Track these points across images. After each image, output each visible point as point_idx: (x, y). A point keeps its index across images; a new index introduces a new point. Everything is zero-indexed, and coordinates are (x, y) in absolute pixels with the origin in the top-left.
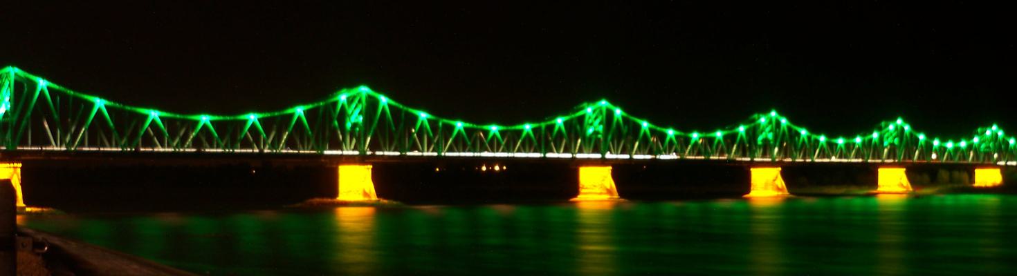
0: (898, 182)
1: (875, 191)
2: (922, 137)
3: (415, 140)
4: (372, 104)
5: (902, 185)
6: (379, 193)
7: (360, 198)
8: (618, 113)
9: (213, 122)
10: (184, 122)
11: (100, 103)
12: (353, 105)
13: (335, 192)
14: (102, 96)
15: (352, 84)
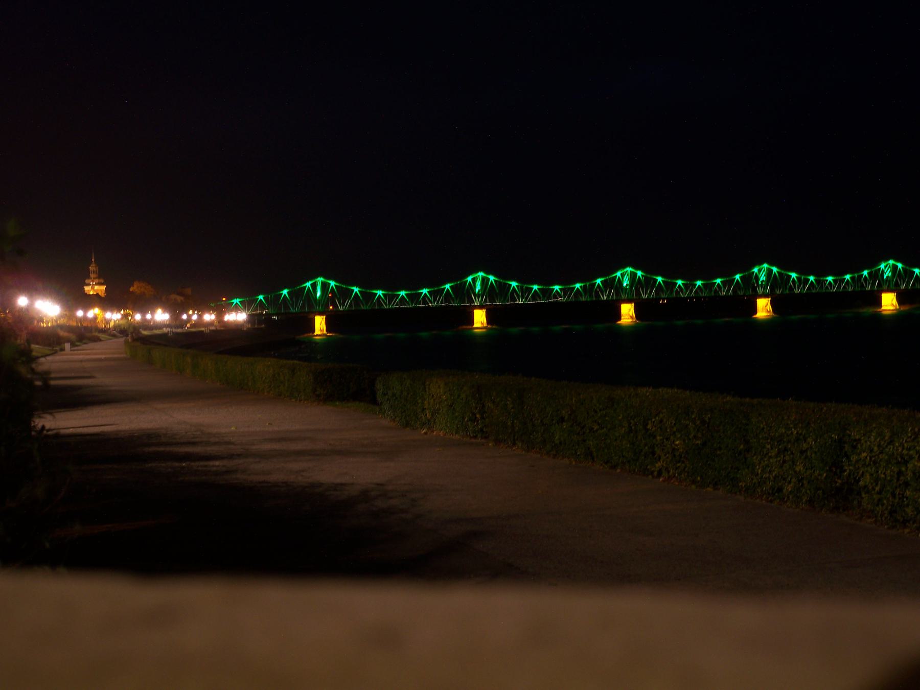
0: (890, 302)
1: (880, 310)
3: (862, 283)
6: (488, 323)
8: (900, 266)
9: (406, 294)
10: (569, 289)
11: (356, 290)
12: (887, 268)
13: (473, 324)
14: (357, 286)
15: (761, 263)
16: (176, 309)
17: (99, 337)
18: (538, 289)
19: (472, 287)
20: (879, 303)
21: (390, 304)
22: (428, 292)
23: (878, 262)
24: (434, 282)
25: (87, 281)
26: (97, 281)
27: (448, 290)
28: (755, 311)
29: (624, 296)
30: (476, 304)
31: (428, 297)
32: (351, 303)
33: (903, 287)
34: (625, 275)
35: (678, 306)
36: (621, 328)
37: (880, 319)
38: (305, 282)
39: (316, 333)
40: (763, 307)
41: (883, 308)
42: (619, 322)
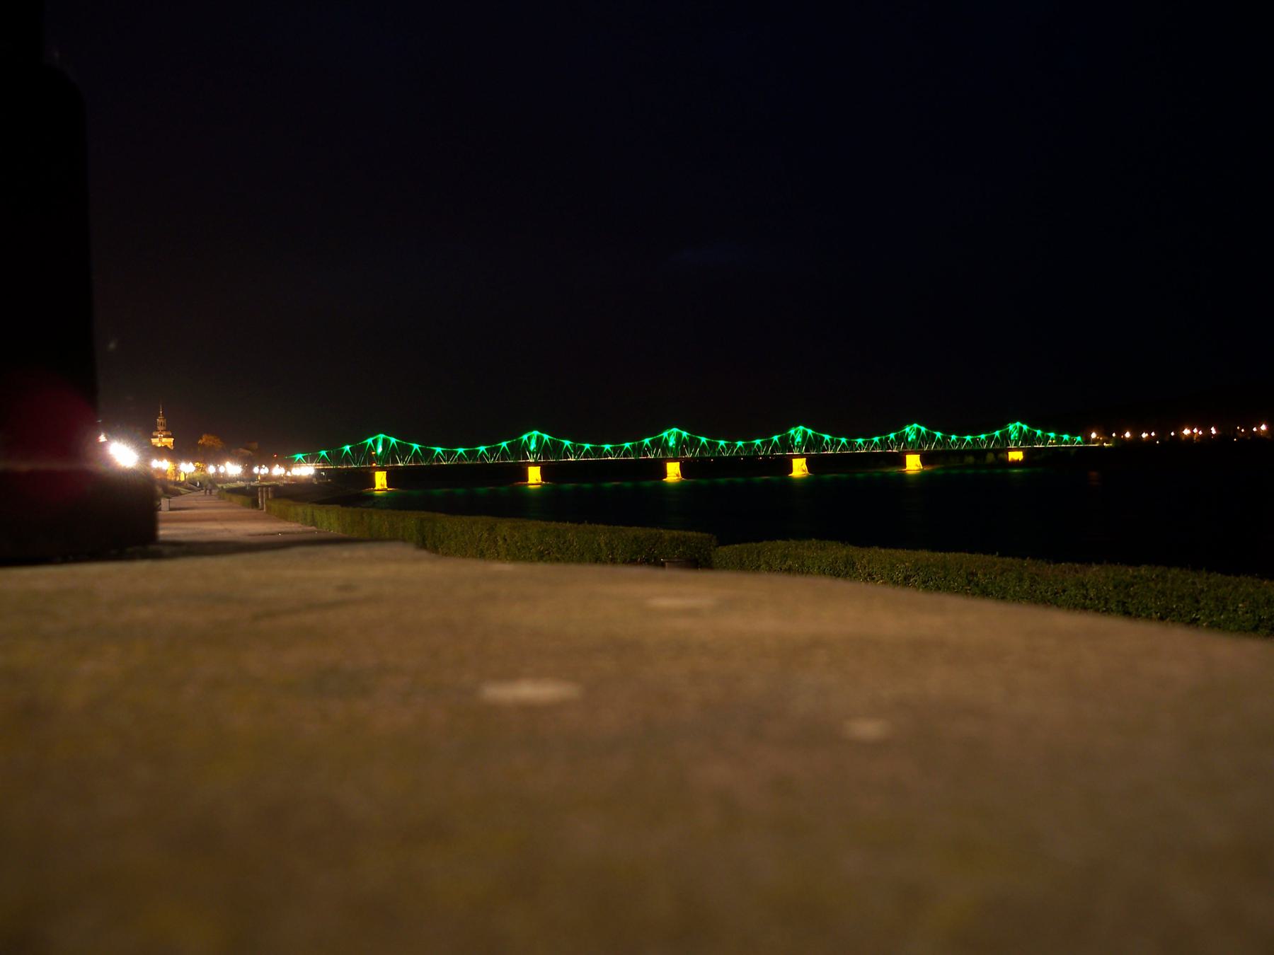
0: (914, 464)
2: (1039, 432)
4: (805, 433)
5: (917, 465)
7: (535, 482)
8: (923, 429)
9: (465, 452)
11: (416, 446)
13: (527, 480)
15: (796, 425)
16: (249, 462)
17: (179, 491)
18: (591, 447)
19: (527, 446)
20: (903, 464)
21: (448, 461)
22: (486, 449)
23: (902, 426)
24: (491, 440)
25: (154, 434)
26: (164, 433)
27: (504, 448)
28: (665, 475)
29: (670, 456)
30: (531, 461)
31: (485, 455)
32: (411, 458)
33: (926, 449)
34: (671, 436)
35: (1058, 456)
36: (793, 480)
37: (903, 477)
38: (366, 438)
39: (376, 488)
40: (799, 468)
41: (907, 468)
42: (664, 480)
